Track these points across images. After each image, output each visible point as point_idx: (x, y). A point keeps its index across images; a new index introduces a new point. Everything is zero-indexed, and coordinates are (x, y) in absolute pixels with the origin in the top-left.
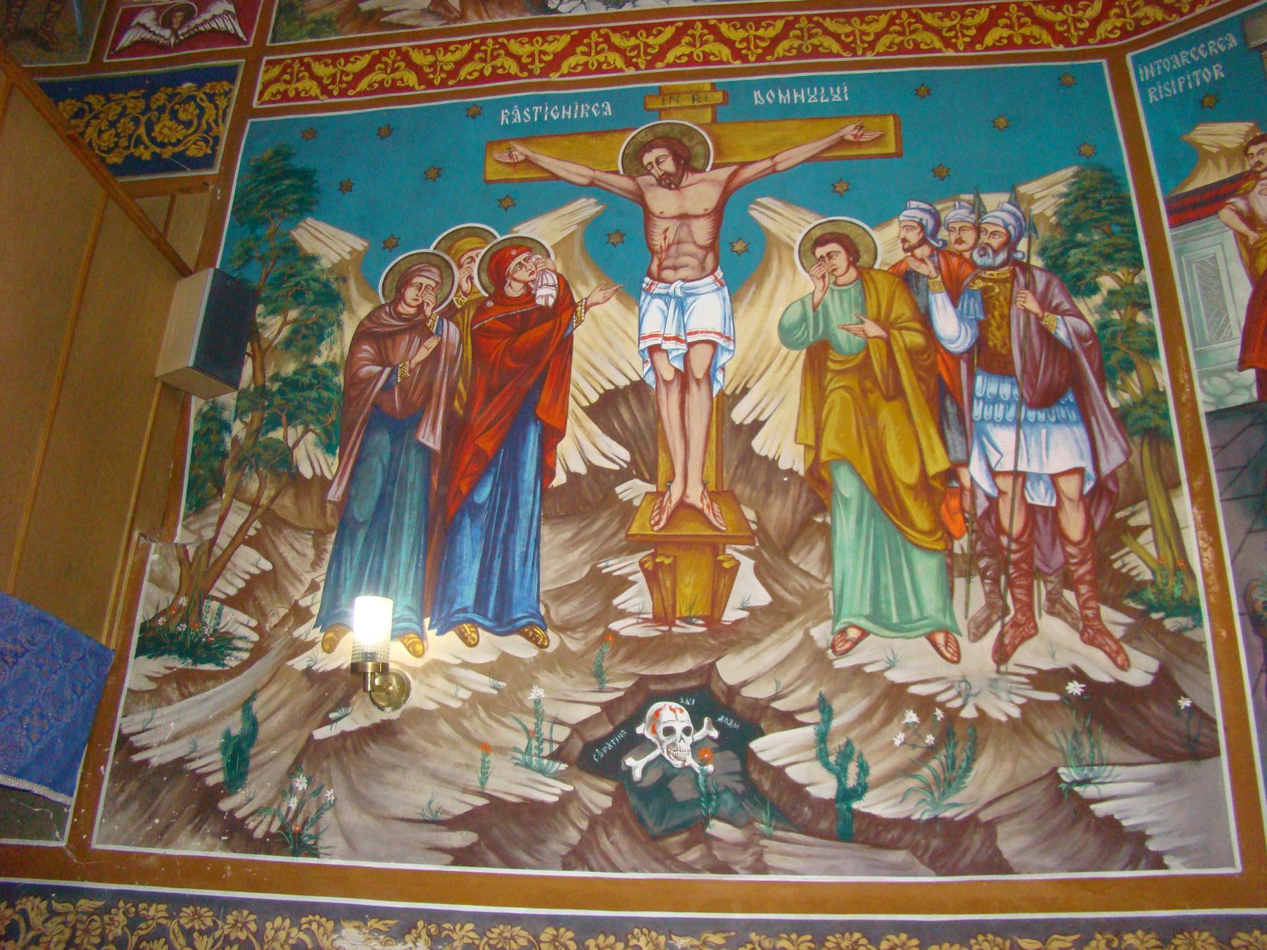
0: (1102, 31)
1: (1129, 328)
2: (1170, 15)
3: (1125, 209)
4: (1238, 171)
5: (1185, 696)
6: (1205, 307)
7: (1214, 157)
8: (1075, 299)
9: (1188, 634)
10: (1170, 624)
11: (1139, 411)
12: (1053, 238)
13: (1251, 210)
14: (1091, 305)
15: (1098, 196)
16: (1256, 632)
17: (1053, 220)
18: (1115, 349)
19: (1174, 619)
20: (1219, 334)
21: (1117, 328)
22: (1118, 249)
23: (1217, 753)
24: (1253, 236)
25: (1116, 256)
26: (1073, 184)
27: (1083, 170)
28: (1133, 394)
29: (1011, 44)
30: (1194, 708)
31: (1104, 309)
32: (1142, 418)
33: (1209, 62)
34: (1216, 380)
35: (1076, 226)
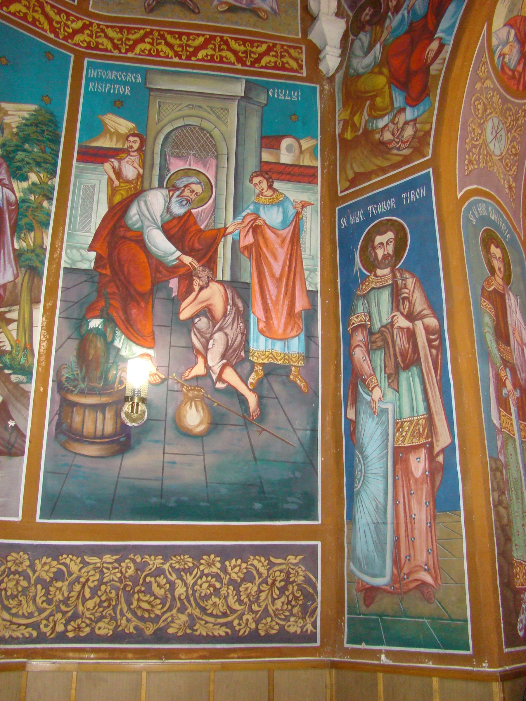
0: (78, 38)
1: (37, 208)
2: (114, 49)
3: (56, 140)
4: (121, 147)
5: (13, 420)
6: (81, 210)
7: (111, 134)
8: (12, 180)
9: (22, 385)
10: (14, 378)
11: (29, 255)
12: (11, 140)
13: (120, 169)
14: (20, 187)
15: (44, 128)
16: (59, 392)
17: (15, 130)
18: (27, 216)
19: (16, 376)
20: (84, 228)
21: (31, 205)
22: (46, 161)
23: (23, 454)
24: (116, 183)
25: (43, 165)
26: (32, 115)
27: (40, 109)
28: (28, 245)
29: (25, 18)
30: (16, 427)
31: (27, 192)
32: (30, 259)
33: (126, 84)
34: (74, 251)
35: (26, 139)
